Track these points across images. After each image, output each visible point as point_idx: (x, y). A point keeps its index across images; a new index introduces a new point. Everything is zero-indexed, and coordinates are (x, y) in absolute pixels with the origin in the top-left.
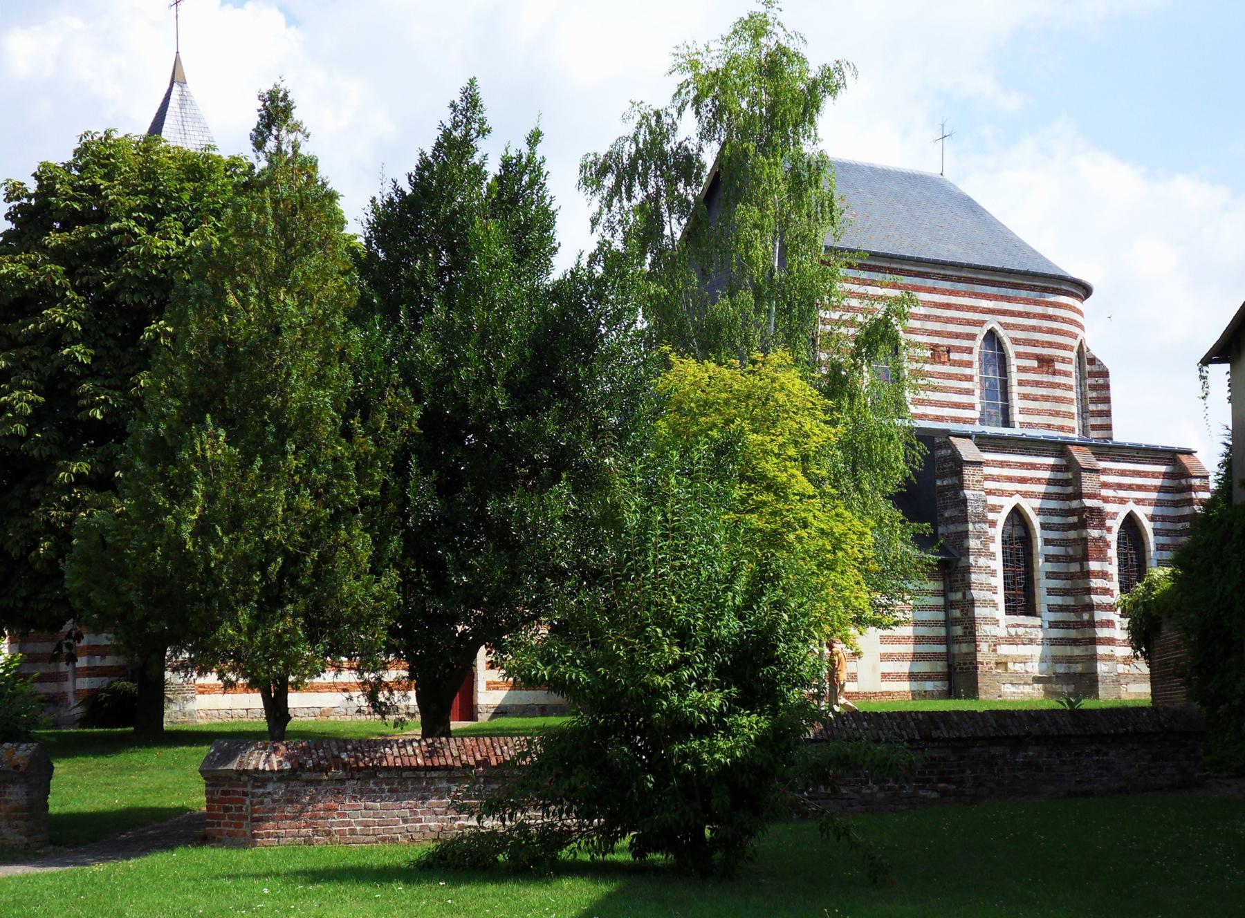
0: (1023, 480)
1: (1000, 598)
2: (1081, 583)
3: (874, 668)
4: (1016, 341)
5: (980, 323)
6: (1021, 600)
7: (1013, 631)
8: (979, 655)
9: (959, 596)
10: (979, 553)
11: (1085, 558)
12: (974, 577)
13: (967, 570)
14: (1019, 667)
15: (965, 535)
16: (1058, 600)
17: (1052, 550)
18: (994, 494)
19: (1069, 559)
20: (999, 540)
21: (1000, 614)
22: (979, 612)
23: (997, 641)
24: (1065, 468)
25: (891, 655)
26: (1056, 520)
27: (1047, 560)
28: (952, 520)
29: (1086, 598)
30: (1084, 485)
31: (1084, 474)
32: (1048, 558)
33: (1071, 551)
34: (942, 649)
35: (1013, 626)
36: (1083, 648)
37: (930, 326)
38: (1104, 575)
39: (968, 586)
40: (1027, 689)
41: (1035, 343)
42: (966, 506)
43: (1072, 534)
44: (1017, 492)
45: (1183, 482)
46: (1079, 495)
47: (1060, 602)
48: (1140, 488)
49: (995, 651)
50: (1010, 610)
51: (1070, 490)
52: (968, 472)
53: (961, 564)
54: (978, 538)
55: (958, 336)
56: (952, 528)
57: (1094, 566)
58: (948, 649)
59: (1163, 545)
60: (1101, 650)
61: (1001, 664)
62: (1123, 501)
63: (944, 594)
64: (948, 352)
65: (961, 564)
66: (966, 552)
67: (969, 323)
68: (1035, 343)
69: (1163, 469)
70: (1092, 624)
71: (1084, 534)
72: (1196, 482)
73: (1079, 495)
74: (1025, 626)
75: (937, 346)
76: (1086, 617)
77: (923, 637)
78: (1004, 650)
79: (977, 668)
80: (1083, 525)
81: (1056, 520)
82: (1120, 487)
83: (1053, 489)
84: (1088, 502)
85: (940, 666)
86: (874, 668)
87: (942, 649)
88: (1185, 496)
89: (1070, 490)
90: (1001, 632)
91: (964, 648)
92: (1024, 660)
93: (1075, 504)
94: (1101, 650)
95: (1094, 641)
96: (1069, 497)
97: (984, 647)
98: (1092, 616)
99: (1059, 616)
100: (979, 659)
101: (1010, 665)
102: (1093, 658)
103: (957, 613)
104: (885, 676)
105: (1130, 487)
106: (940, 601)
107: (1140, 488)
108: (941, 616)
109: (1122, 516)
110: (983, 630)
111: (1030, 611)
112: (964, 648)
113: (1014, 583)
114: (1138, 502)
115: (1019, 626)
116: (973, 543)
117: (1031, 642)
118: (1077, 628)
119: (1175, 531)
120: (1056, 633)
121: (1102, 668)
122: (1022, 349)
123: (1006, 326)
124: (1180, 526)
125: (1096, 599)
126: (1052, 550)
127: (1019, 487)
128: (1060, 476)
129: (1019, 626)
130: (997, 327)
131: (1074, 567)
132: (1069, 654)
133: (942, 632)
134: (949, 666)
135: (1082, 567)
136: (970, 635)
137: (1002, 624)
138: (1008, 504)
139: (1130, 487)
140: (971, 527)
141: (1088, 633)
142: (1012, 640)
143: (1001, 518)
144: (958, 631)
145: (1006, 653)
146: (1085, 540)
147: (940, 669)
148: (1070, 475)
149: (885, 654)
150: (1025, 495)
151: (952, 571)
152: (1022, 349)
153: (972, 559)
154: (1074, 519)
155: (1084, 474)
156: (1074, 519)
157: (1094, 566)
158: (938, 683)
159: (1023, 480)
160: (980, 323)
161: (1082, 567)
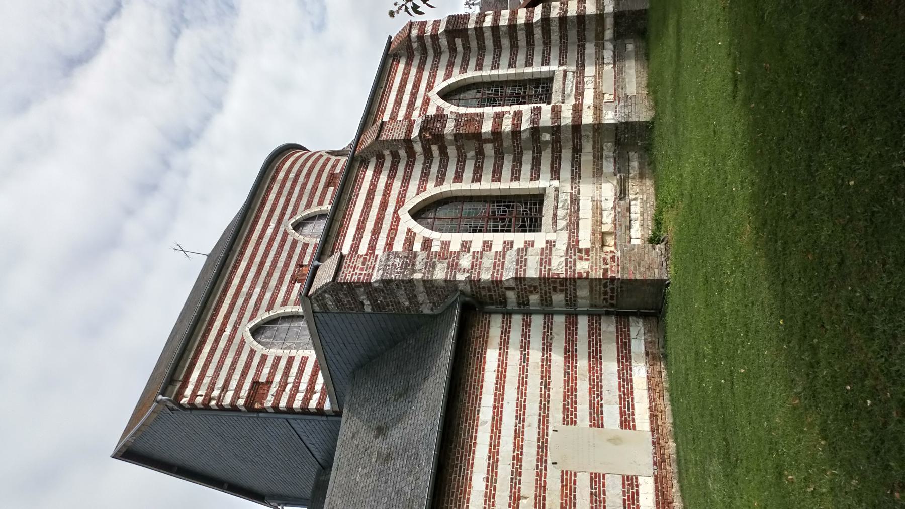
0: (384, 205)
1: (519, 238)
2: (507, 143)
3: (615, 440)
4: (309, 205)
5: (285, 234)
6: (523, 212)
7: (561, 223)
8: (593, 275)
9: (511, 296)
10: (454, 267)
11: (477, 136)
12: (486, 276)
13: (474, 283)
14: (608, 218)
15: (429, 285)
16: (526, 169)
17: (468, 174)
18: (393, 239)
19: (480, 155)
20: (446, 236)
21: (539, 239)
22: (532, 272)
23: (573, 246)
24: (380, 157)
25: (592, 406)
26: (435, 169)
27: (479, 180)
28: (412, 298)
29: (524, 136)
30: (396, 137)
31: (384, 137)
32: (477, 179)
33: (471, 154)
34: (583, 322)
35: (555, 222)
36: (584, 142)
37: (273, 283)
38: (499, 117)
39: (496, 283)
40: (636, 209)
41: (315, 188)
42: (391, 281)
43: (452, 151)
44: (395, 212)
45: (415, 45)
46: (408, 142)
47: (529, 167)
48: (416, 86)
49: (587, 251)
50: (534, 225)
51: (402, 153)
52: (350, 275)
53: (468, 289)
54: (434, 266)
55: (290, 257)
56: (422, 298)
57: (487, 127)
58: (583, 313)
59: (477, 64)
60: (588, 118)
61: (601, 238)
62: (427, 102)
63: (508, 314)
64: (302, 266)
65: (468, 289)
66: (451, 284)
67: (283, 240)
68: (315, 188)
69: (402, 66)
70: (556, 130)
71: (450, 138)
72: (415, 33)
73: (408, 142)
74: (556, 208)
75: (293, 277)
76: (547, 137)
77: (566, 350)
78: (585, 241)
79: (613, 280)
80: (439, 138)
81: (435, 169)
82: (411, 104)
83: (400, 173)
84: (415, 133)
85: (609, 327)
86: (615, 440)
87: (583, 322)
88: (429, 42)
89: (402, 153)
90: (562, 240)
91: (583, 293)
92: (598, 210)
93: (418, 148)
94: (588, 118)
95: (577, 127)
96: (411, 154)
97: (583, 267)
98: (546, 129)
99: (545, 167)
100: (600, 275)
101: (605, 228)
102: (598, 128)
103: (534, 298)
104: (627, 422)
105: (414, 96)
106: (517, 320)
107: (416, 86)
108: (537, 321)
109: (441, 102)
110: (558, 266)
111: (537, 199)
112: (583, 293)
113: (503, 219)
114: (430, 87)
115: (555, 216)
116: (440, 274)
117: (575, 200)
118: (563, 145)
119: (464, 54)
120: (566, 171)
121: (609, 117)
122: (316, 200)
123: (294, 213)
124: (460, 48)
125: (525, 125)
126: (468, 174)
127: (390, 210)
128: (387, 164)
129: (555, 216)
130: (293, 220)
131: (489, 149)
132: (591, 158)
133: (559, 320)
134: (608, 313)
135: (487, 141)
136: (567, 284)
137: (551, 236)
138: (407, 222)
139: (414, 96)
140: (418, 276)
141: (566, 136)
142: (573, 227)
143: (421, 231)
144: (558, 298)
145: (589, 232)
146: (457, 136)
147: (613, 328)
148: (386, 152)
149: (592, 418)
150: (400, 202)
151: (476, 307)
152: (316, 200)
153: (460, 277)
154: (435, 148)
155: (384, 137)
156: (435, 148)
157: (487, 127)
158: (633, 332)
159: (384, 205)
160: (285, 234)
161: (487, 141)
